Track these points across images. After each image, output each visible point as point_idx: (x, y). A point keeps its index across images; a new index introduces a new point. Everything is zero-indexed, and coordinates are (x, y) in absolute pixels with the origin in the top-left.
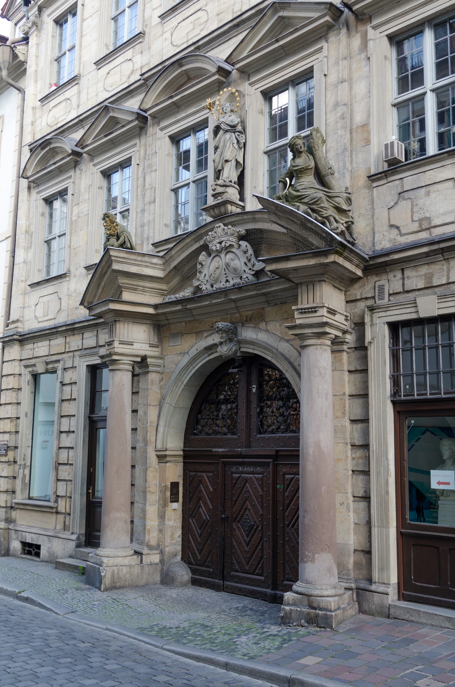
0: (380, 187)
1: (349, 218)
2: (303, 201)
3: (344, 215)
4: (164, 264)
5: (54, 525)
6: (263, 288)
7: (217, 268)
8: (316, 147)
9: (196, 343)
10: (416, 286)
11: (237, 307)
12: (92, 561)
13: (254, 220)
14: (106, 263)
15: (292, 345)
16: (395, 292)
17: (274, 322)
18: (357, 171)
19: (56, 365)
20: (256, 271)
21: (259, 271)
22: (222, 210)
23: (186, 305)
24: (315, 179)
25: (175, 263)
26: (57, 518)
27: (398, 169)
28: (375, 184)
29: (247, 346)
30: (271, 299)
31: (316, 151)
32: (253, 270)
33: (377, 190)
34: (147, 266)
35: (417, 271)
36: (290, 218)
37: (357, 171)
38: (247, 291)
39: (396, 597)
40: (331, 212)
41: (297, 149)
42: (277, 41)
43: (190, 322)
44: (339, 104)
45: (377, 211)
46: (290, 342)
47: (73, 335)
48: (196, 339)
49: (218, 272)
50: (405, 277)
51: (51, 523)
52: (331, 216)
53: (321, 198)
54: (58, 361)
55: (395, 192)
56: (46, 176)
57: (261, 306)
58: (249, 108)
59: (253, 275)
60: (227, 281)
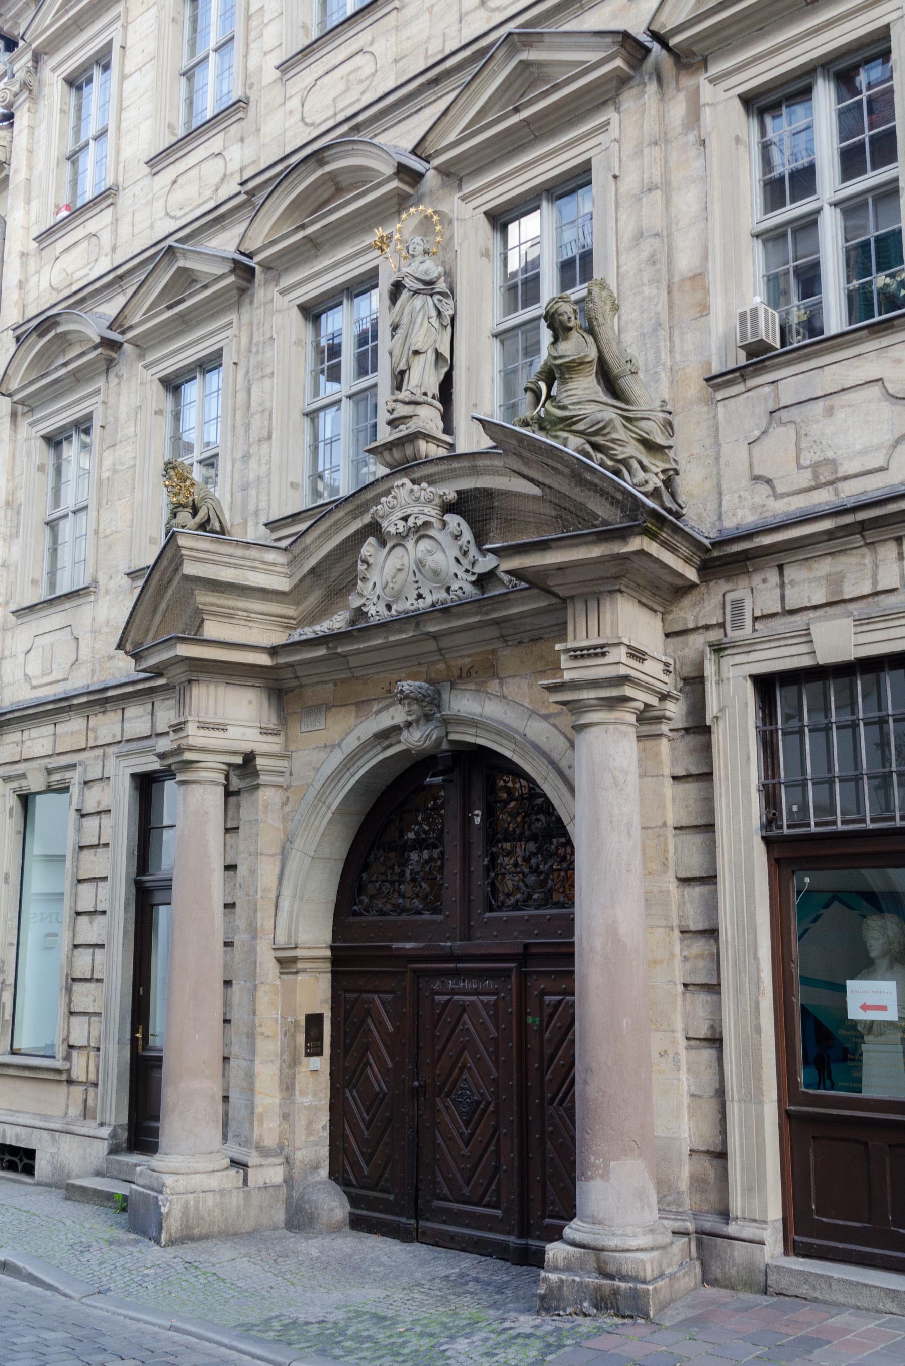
0: (732, 400)
1: (669, 462)
2: (574, 428)
3: (659, 455)
4: (289, 564)
5: (64, 1107)
6: (494, 610)
7: (400, 570)
8: (601, 319)
9: (356, 726)
10: (810, 601)
11: (440, 650)
12: (141, 1182)
13: (475, 472)
14: (171, 563)
15: (554, 726)
16: (765, 613)
17: (517, 680)
18: (684, 369)
19: (68, 775)
20: (480, 575)
21: (485, 574)
22: (409, 451)
23: (336, 648)
24: (599, 384)
25: (313, 562)
26: (69, 1094)
27: (767, 363)
28: (720, 395)
29: (462, 729)
30: (511, 631)
31: (599, 326)
32: (473, 574)
33: (725, 406)
34: (254, 569)
35: (810, 569)
36: (550, 462)
37: (684, 369)
38: (459, 616)
39: (780, 1248)
40: (632, 450)
41: (561, 322)
42: (517, 110)
43: (343, 681)
44: (646, 234)
45: (725, 449)
46: (552, 720)
47: (103, 712)
48: (357, 717)
49: (401, 577)
50: (786, 581)
51: (58, 1103)
52: (632, 457)
53: (611, 421)
54: (73, 766)
55: (762, 409)
56: (49, 391)
57: (490, 648)
58: (460, 245)
59: (473, 583)
60: (420, 596)
